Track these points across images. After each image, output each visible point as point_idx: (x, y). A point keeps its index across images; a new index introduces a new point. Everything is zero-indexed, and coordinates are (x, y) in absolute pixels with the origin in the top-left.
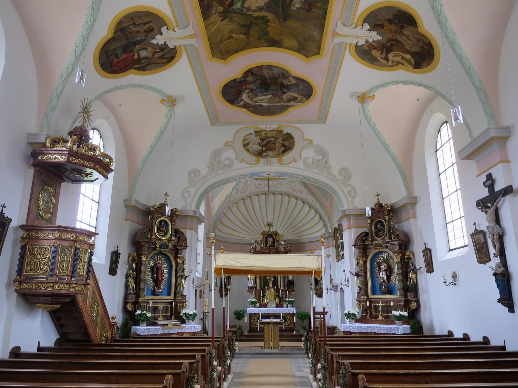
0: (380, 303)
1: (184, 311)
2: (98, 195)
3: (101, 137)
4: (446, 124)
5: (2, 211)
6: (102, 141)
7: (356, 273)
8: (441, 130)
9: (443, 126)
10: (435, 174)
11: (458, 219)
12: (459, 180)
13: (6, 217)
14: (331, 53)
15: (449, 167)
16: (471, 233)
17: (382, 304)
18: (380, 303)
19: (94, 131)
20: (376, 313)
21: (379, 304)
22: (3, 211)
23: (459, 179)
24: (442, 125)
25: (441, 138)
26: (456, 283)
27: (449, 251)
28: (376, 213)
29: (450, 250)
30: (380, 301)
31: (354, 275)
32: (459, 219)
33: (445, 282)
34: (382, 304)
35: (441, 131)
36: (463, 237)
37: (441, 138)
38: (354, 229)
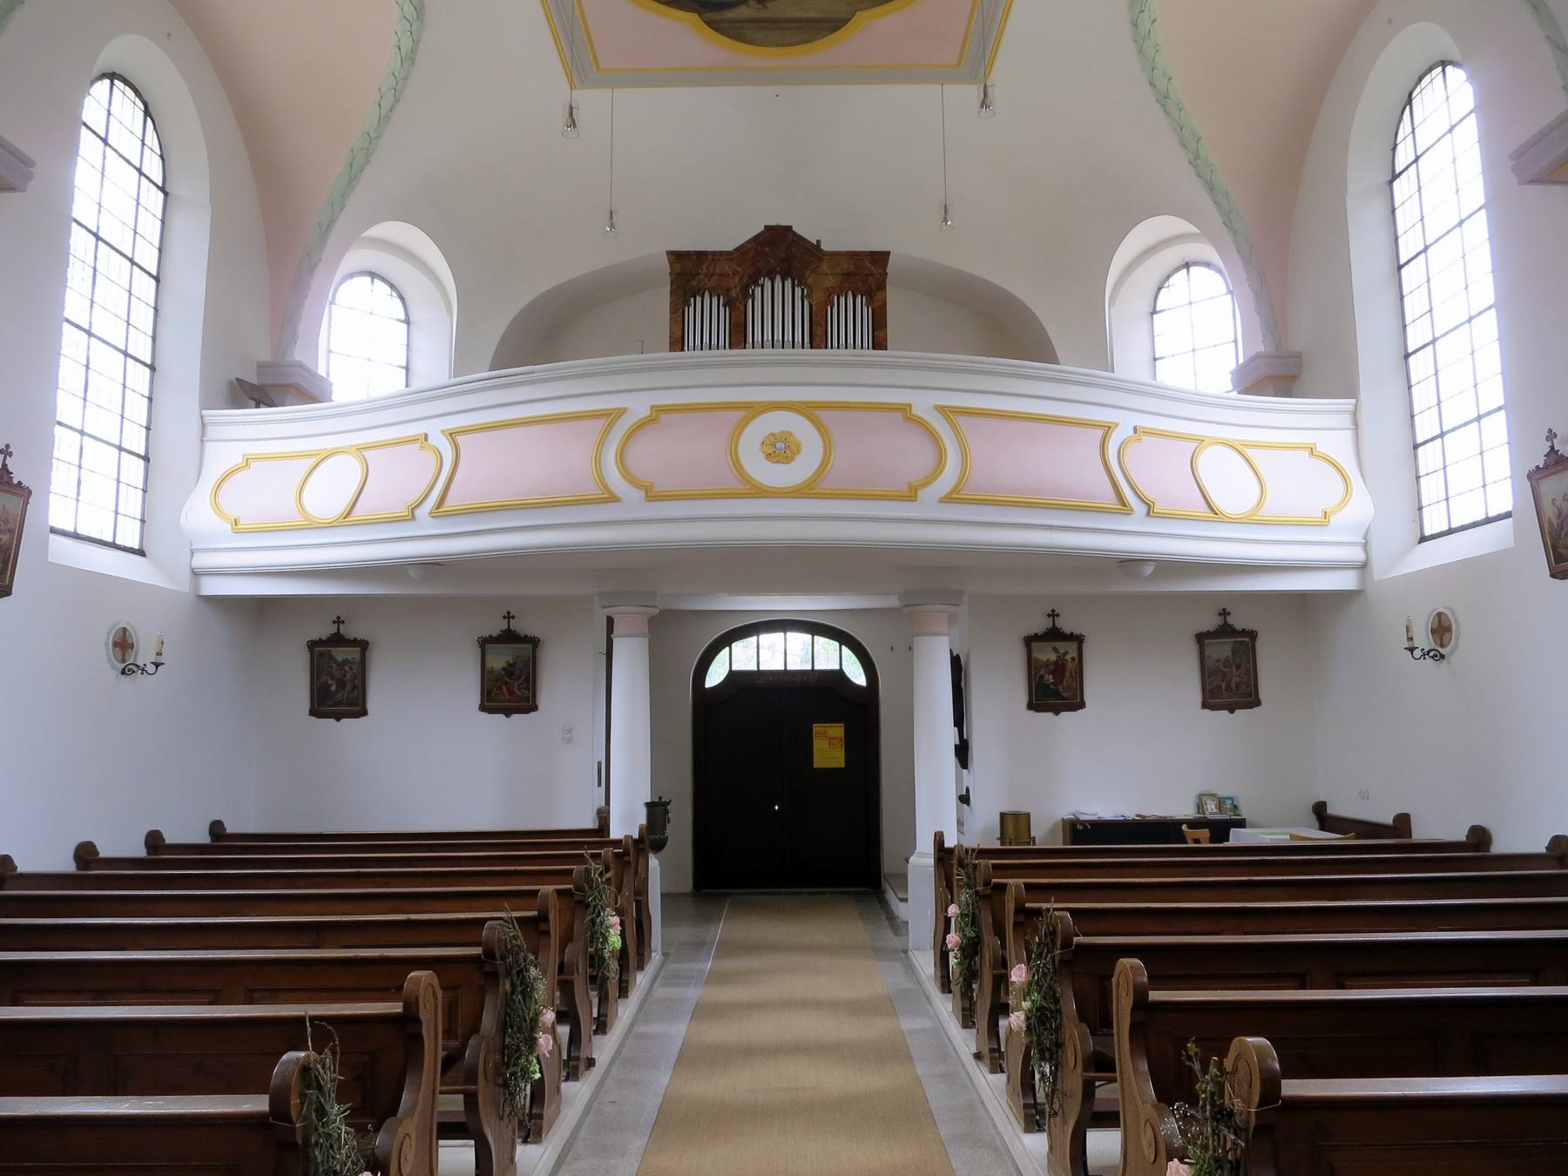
2: (150, 341)
3: (147, 113)
4: (1440, 69)
5: (4, 466)
6: (155, 128)
8: (1414, 95)
9: (1427, 79)
10: (1383, 265)
11: (1454, 429)
12: (1492, 272)
13: (15, 482)
15: (1442, 240)
16: (1533, 467)
19: (112, 84)
22: (6, 465)
23: (1493, 267)
24: (1420, 79)
25: (1413, 129)
26: (1443, 651)
27: (1419, 543)
29: (1423, 539)
32: (1450, 428)
33: (1412, 650)
35: (1414, 101)
36: (1445, 502)
37: (1413, 129)
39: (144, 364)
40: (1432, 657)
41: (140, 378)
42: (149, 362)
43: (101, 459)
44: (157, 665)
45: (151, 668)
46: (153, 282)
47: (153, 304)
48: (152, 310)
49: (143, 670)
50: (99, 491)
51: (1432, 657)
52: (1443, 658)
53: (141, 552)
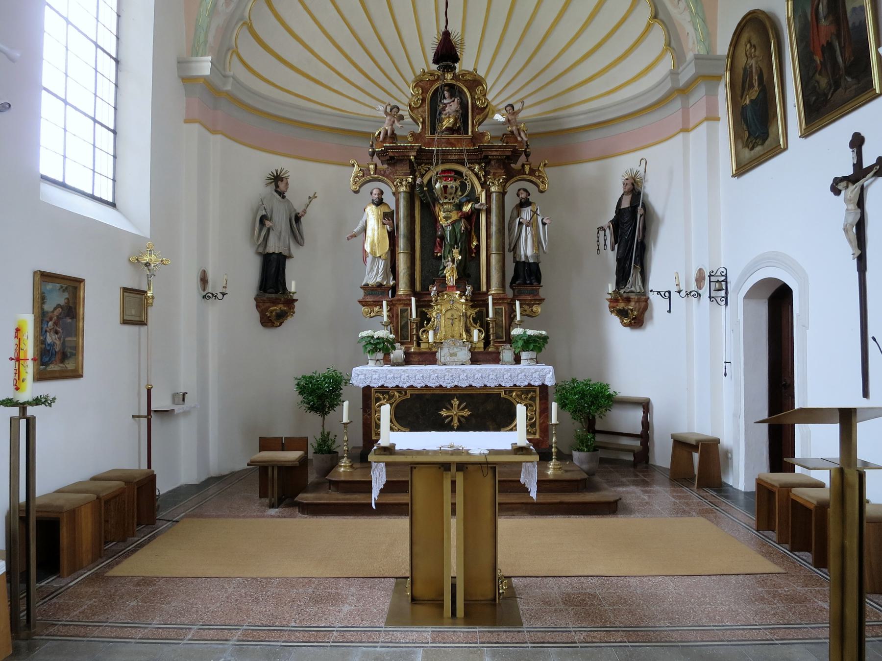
26: (700, 292)
39: (111, 57)
40: (693, 295)
41: (106, 139)
42: (112, 127)
43: (82, 126)
44: (223, 294)
45: (220, 296)
46: (111, 135)
47: (112, 153)
48: (114, 86)
49: (216, 297)
50: (80, 152)
51: (693, 295)
52: (700, 296)
53: (113, 205)
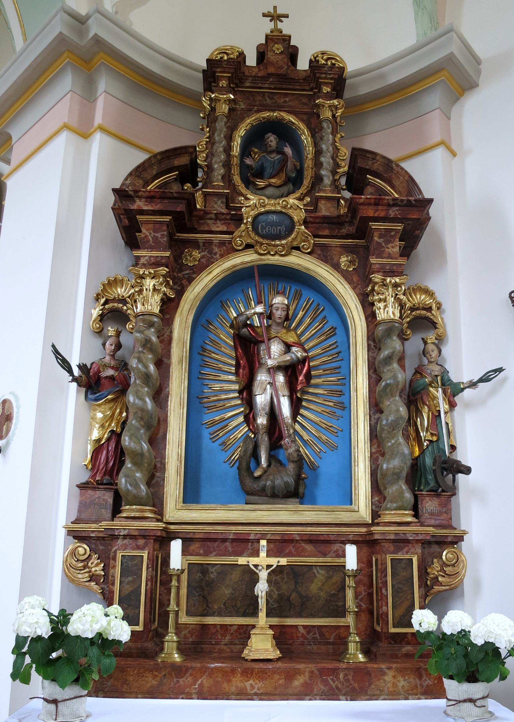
0: (263, 554)
1: (364, 566)
7: (82, 367)
14: (23, 55)
17: (274, 561)
18: (263, 554)
20: (204, 615)
21: (253, 561)
28: (264, 78)
30: (263, 543)
31: (75, 379)
34: (274, 561)
38: (109, 141)
